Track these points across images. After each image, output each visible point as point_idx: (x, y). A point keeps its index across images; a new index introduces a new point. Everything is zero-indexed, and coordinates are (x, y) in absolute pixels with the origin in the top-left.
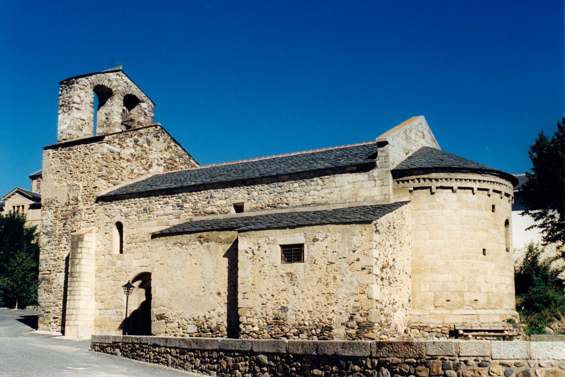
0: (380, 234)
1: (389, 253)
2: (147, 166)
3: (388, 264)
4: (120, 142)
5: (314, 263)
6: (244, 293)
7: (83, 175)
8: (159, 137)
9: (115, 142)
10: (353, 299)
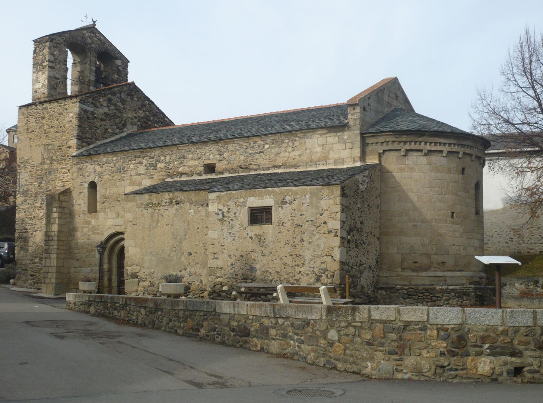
0: (347, 197)
1: (357, 217)
3: (355, 227)
4: (94, 102)
5: (282, 225)
6: (214, 254)
7: (57, 135)
8: (133, 96)
9: (89, 102)
10: (319, 261)
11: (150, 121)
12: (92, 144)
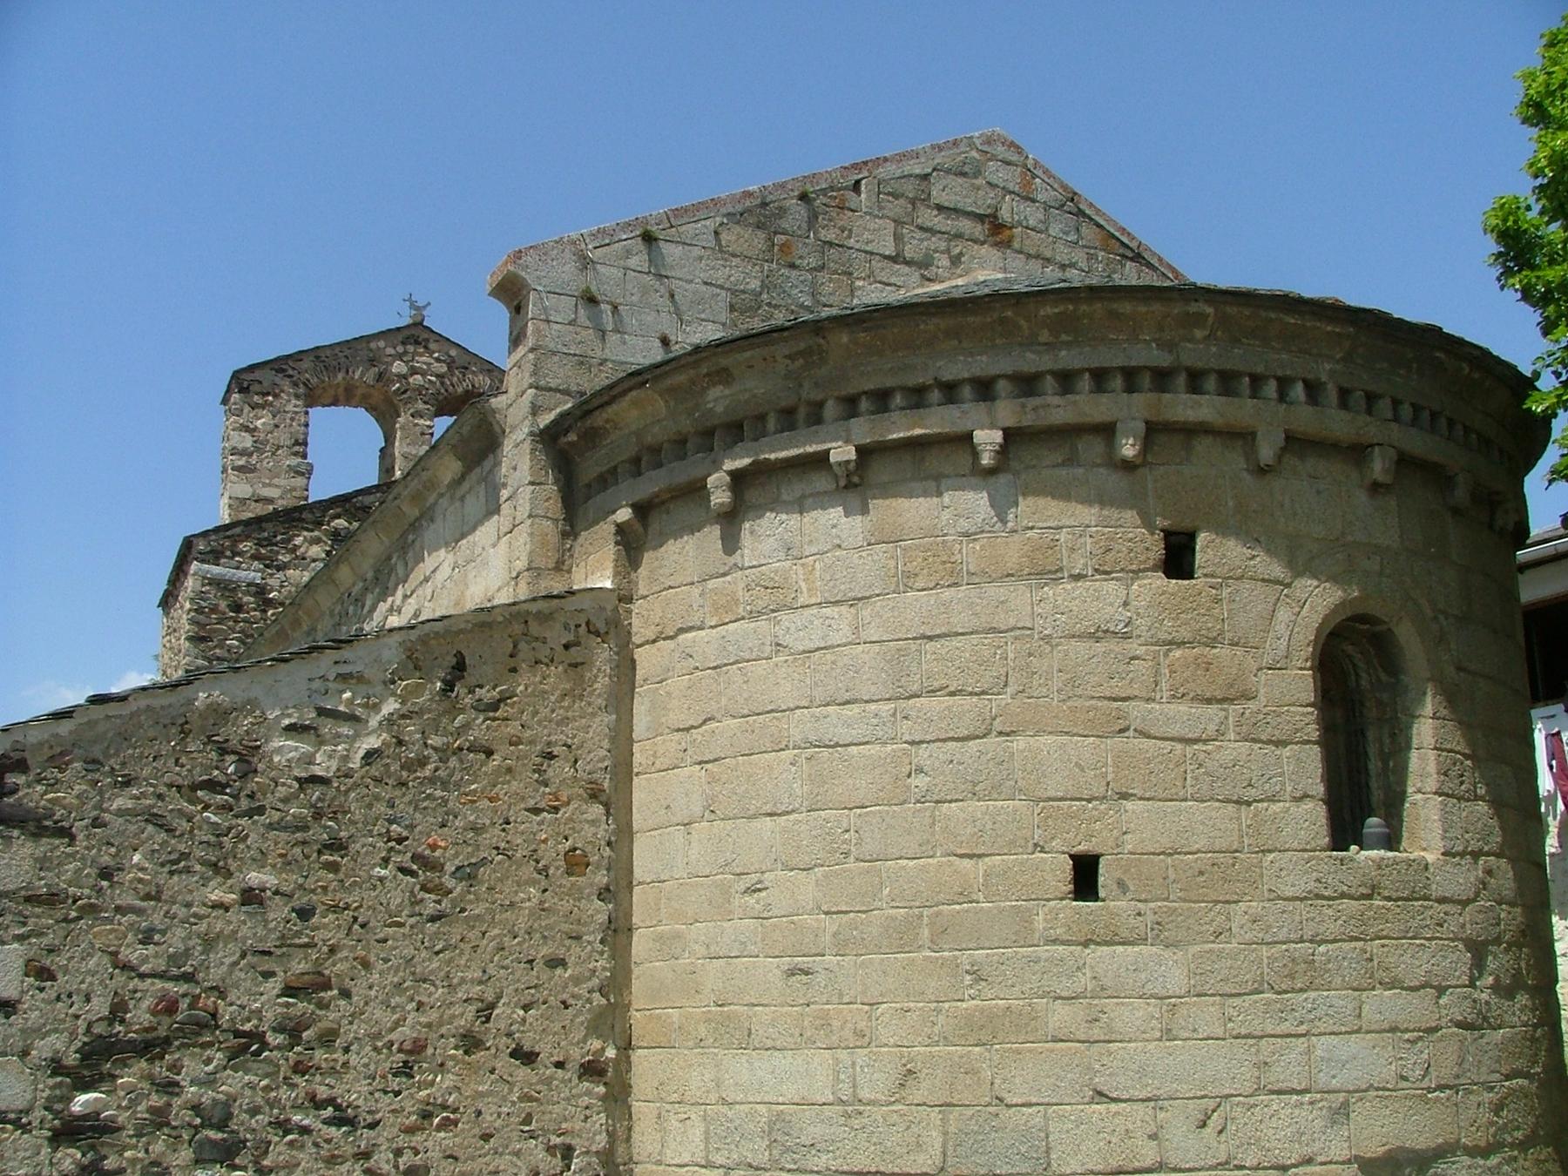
9: (240, 554)
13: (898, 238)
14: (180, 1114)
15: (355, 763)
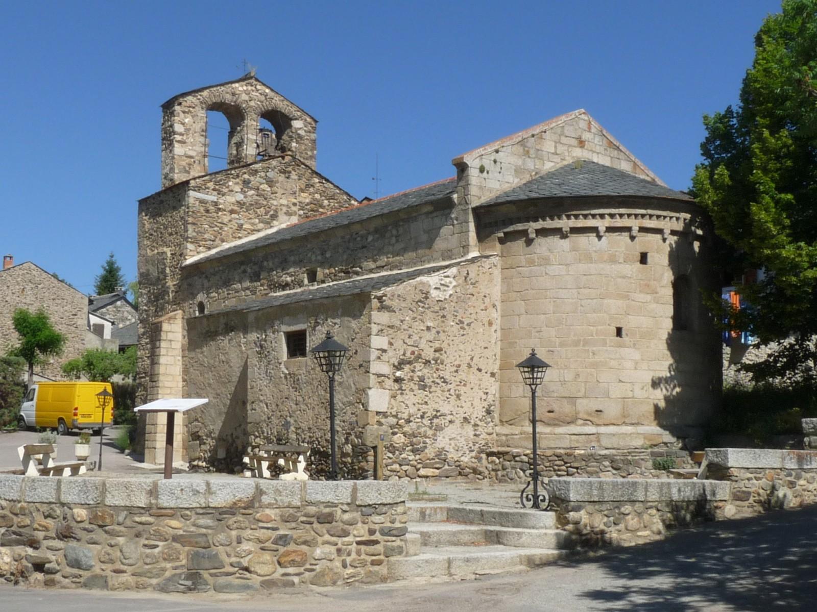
2: (268, 217)
4: (217, 187)
8: (290, 172)
9: (208, 188)
11: (323, 207)
12: (214, 248)
13: (556, 147)
14: (416, 379)
15: (447, 297)
